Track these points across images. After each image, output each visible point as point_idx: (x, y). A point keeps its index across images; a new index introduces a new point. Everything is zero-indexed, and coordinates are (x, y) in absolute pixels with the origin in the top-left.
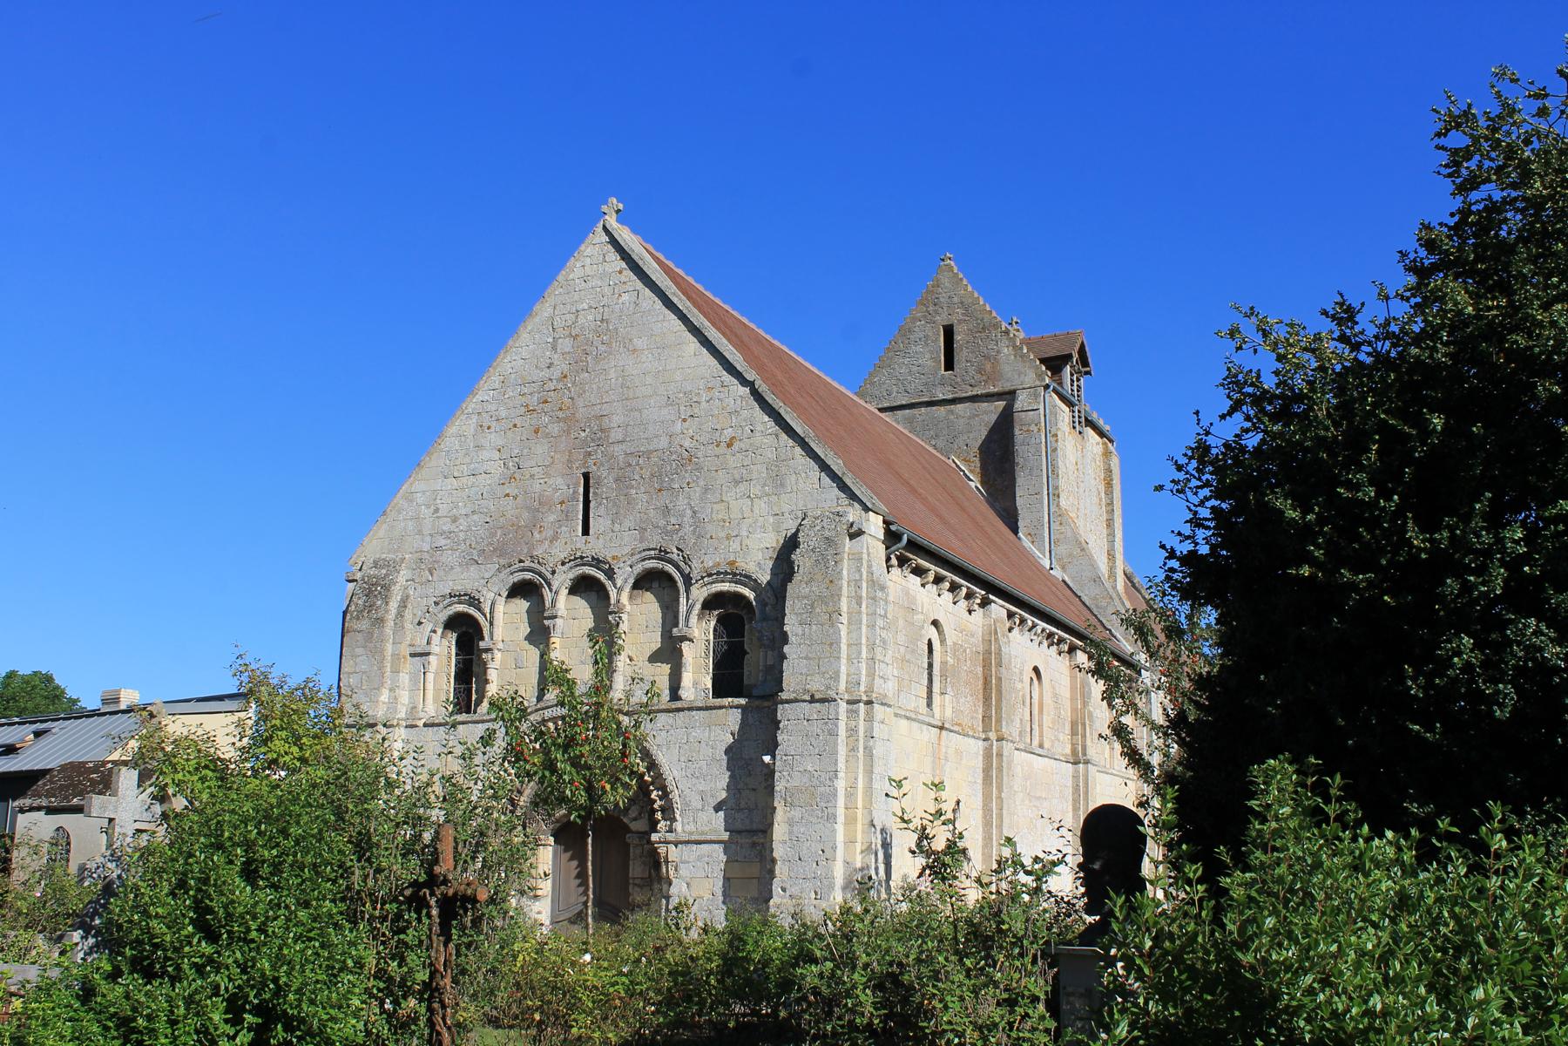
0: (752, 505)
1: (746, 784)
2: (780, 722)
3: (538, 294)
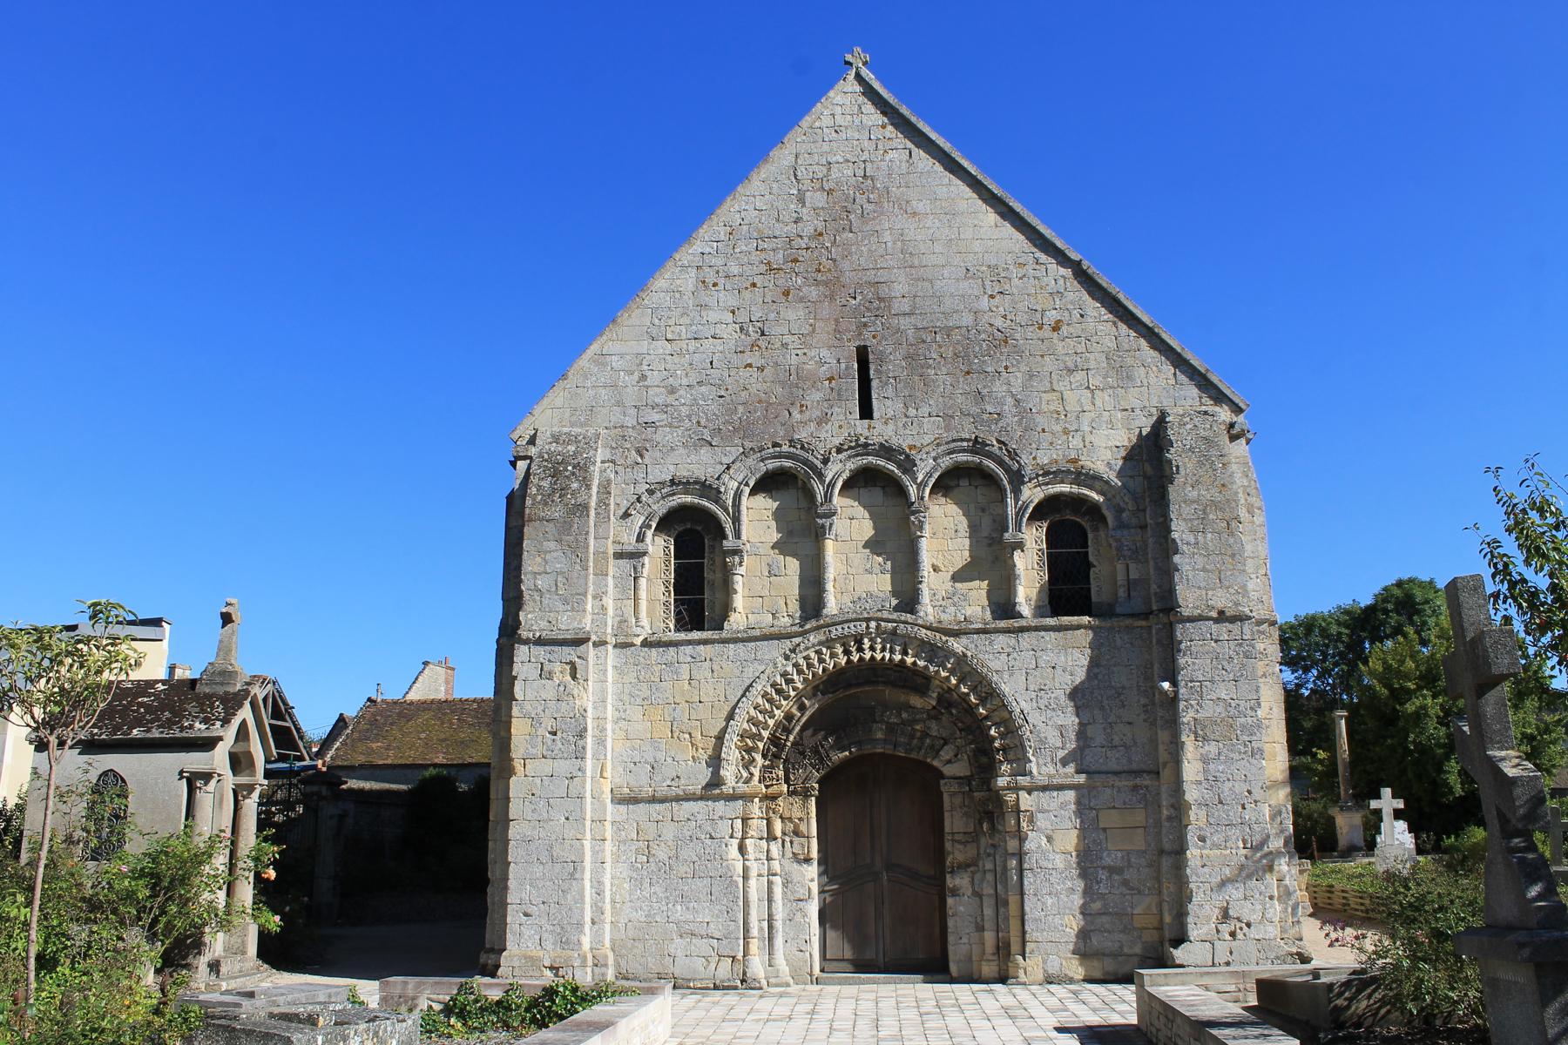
0: (1093, 398)
1: (1119, 717)
2: (1181, 642)
3: (777, 139)
